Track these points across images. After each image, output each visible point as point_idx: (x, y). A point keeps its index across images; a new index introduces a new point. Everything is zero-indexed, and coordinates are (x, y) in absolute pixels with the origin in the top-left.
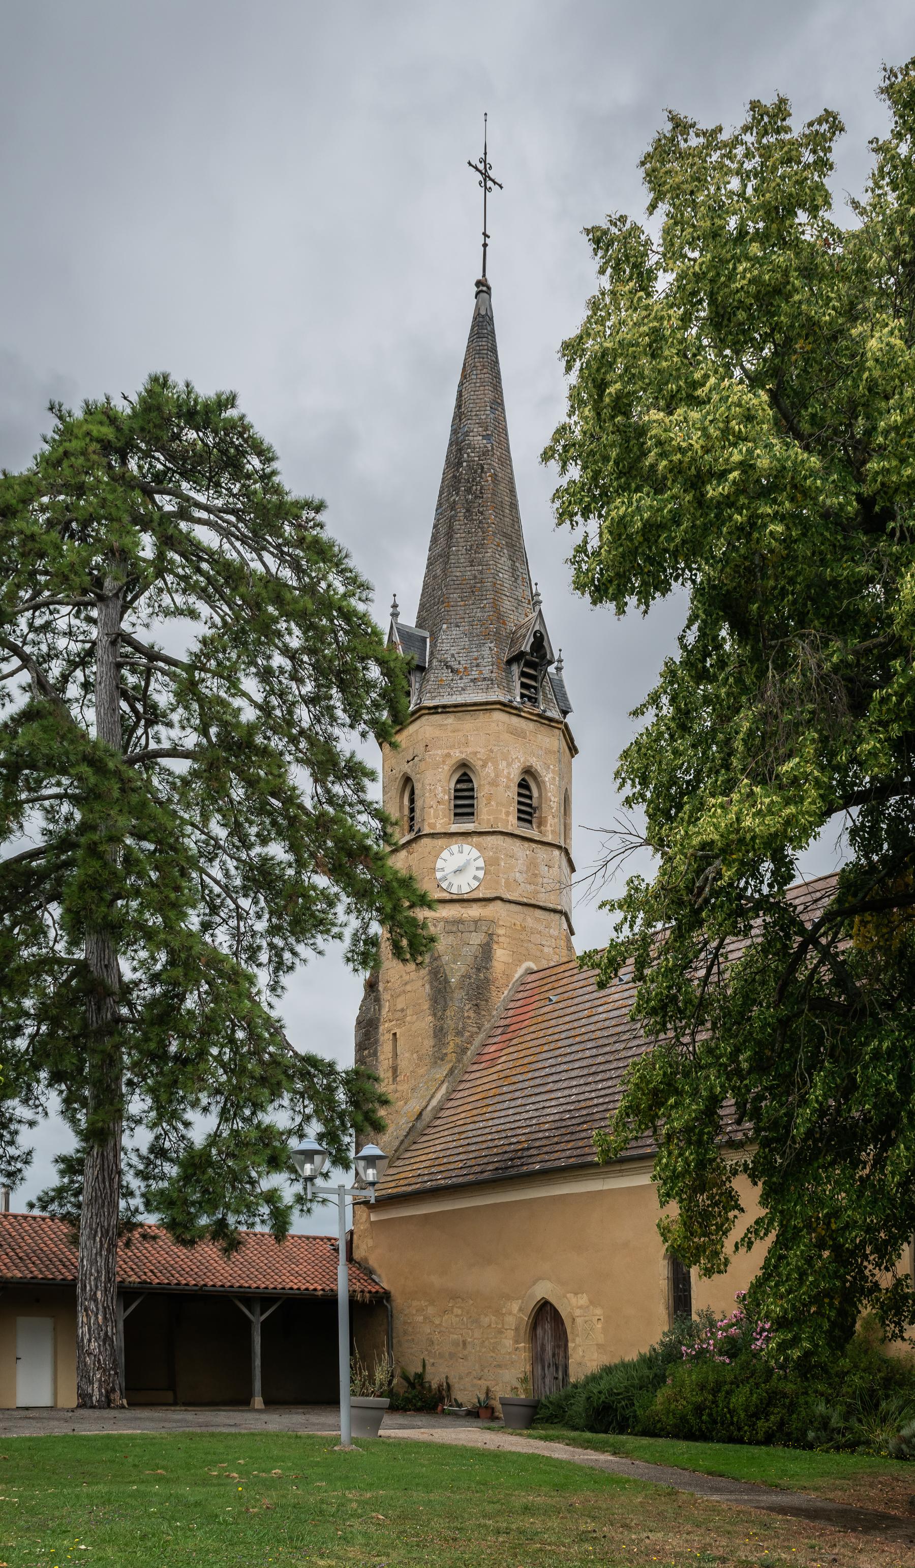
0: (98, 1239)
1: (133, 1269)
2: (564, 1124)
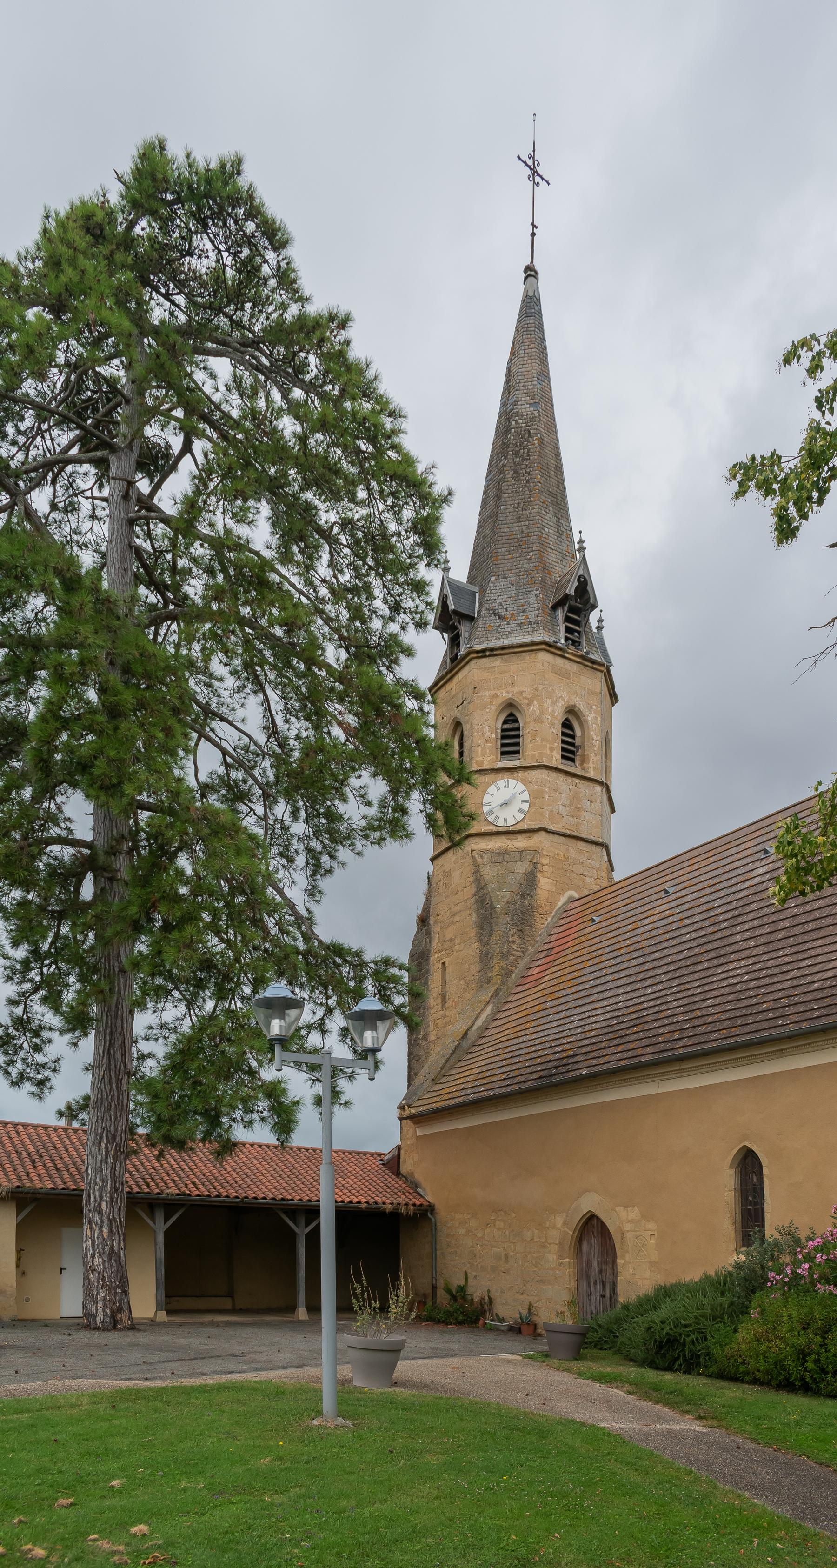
0: (103, 1145)
1: (174, 1181)
2: (612, 1029)
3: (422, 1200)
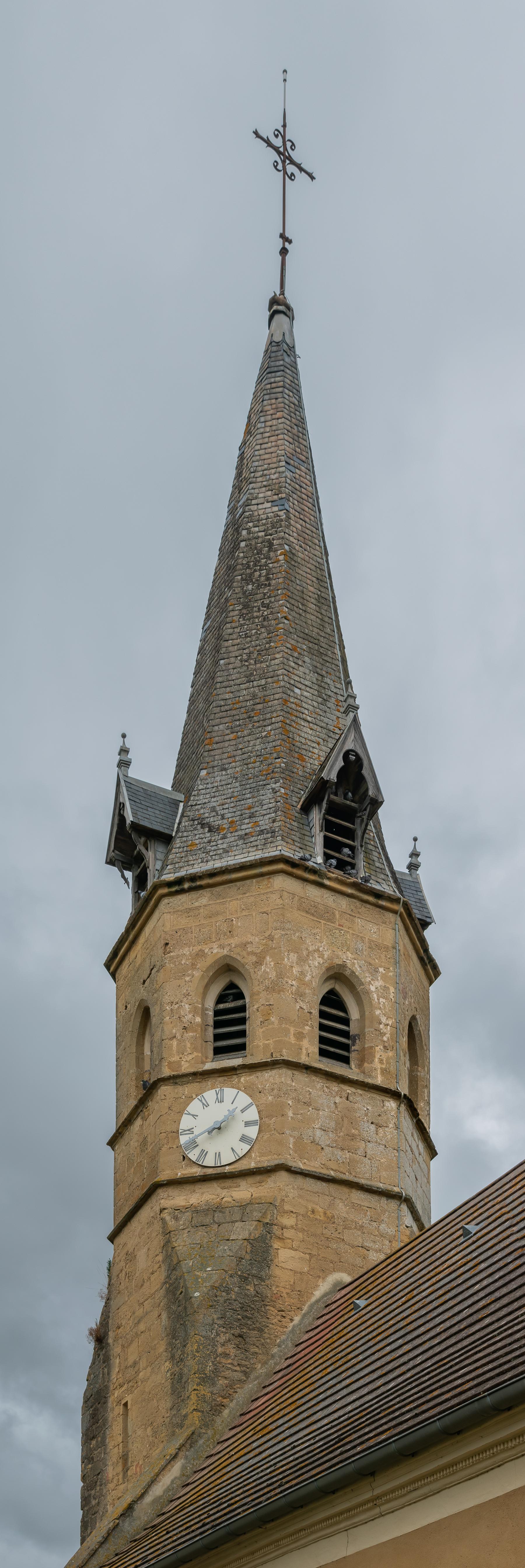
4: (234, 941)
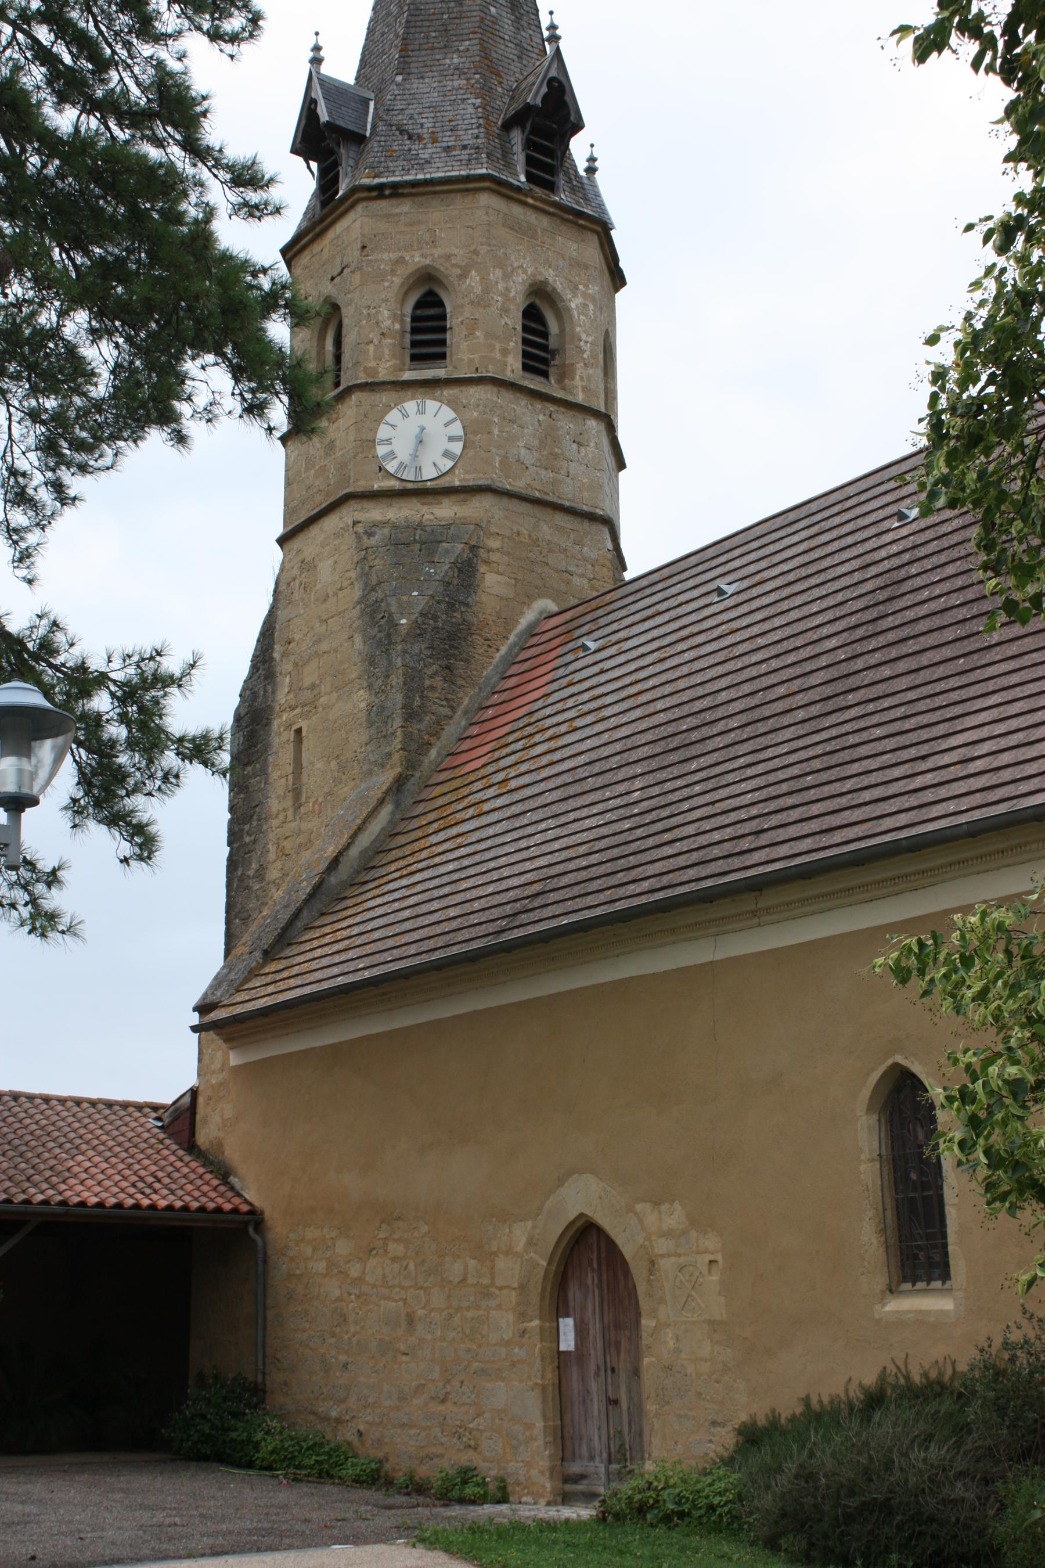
3: (236, 1201)
4: (437, 252)
